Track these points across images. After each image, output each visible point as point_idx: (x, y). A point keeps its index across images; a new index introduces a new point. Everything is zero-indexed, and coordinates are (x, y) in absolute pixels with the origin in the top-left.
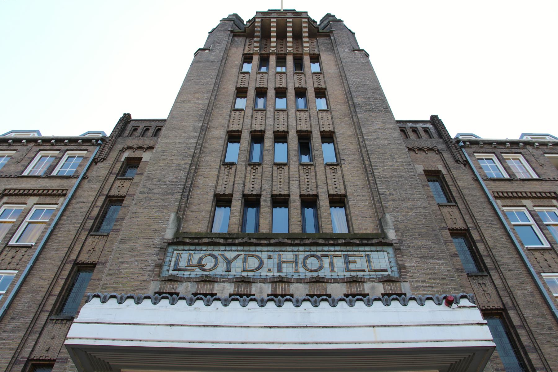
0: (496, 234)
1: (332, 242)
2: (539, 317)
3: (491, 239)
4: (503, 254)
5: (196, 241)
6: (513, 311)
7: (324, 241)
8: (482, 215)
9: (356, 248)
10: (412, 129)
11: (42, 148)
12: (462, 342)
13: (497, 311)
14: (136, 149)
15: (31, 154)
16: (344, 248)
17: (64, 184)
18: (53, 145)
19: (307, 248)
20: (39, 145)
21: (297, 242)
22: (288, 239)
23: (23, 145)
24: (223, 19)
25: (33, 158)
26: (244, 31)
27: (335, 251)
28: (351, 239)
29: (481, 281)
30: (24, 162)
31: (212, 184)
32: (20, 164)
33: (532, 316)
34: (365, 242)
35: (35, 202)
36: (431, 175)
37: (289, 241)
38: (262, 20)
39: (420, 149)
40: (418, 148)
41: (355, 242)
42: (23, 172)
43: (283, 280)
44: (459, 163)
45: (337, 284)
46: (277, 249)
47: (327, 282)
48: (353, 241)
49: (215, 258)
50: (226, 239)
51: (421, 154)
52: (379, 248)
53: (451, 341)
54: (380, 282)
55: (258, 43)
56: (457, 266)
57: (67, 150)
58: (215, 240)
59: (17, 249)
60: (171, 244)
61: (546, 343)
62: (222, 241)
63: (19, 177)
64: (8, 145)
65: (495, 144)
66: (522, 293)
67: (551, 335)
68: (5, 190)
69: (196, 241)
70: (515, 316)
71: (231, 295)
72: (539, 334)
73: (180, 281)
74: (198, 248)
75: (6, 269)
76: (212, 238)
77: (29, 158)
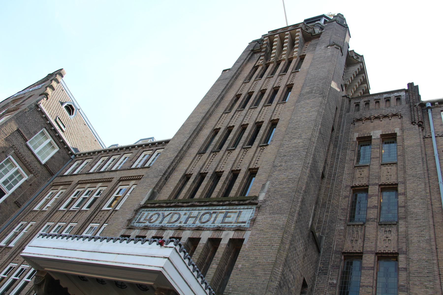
0: (420, 186)
1: (221, 203)
2: (424, 261)
3: (411, 192)
4: (417, 204)
5: (153, 205)
6: (404, 255)
7: (217, 203)
8: (414, 170)
9: (235, 207)
10: (375, 101)
11: (144, 150)
12: (148, 267)
13: (393, 254)
14: (391, 117)
15: (138, 155)
16: (228, 207)
17: (111, 175)
18: (150, 147)
19: (207, 208)
20: (143, 148)
21: (202, 204)
22: (198, 202)
23: (136, 149)
24: (253, 41)
25: (139, 157)
26: (260, 48)
27: (222, 209)
28: (233, 201)
29: (388, 229)
30: (134, 160)
31: (185, 168)
32: (131, 161)
33: (417, 261)
34: (241, 202)
35: (133, 183)
36: (389, 138)
37: (198, 204)
38: (269, 38)
39: (385, 117)
40: (383, 116)
41: (235, 203)
42: (132, 166)
43: (181, 228)
44: (414, 125)
45: (208, 232)
46: (191, 208)
47: (203, 230)
48: (234, 202)
49: (159, 215)
50: (167, 203)
51: (385, 121)
52: (250, 207)
53: (144, 265)
54: (233, 230)
55: (263, 56)
56: (372, 216)
57: (157, 149)
58: (162, 205)
59: (71, 212)
60: (145, 207)
61: (418, 284)
62: (165, 205)
63: (128, 169)
64: (129, 150)
65: (437, 103)
66: (418, 239)
67: (428, 278)
68: (121, 177)
69: (153, 205)
70: (404, 260)
71: (170, 238)
72: (416, 276)
73: (134, 229)
74: (153, 209)
75: (96, 223)
76: (160, 203)
77: (136, 157)
